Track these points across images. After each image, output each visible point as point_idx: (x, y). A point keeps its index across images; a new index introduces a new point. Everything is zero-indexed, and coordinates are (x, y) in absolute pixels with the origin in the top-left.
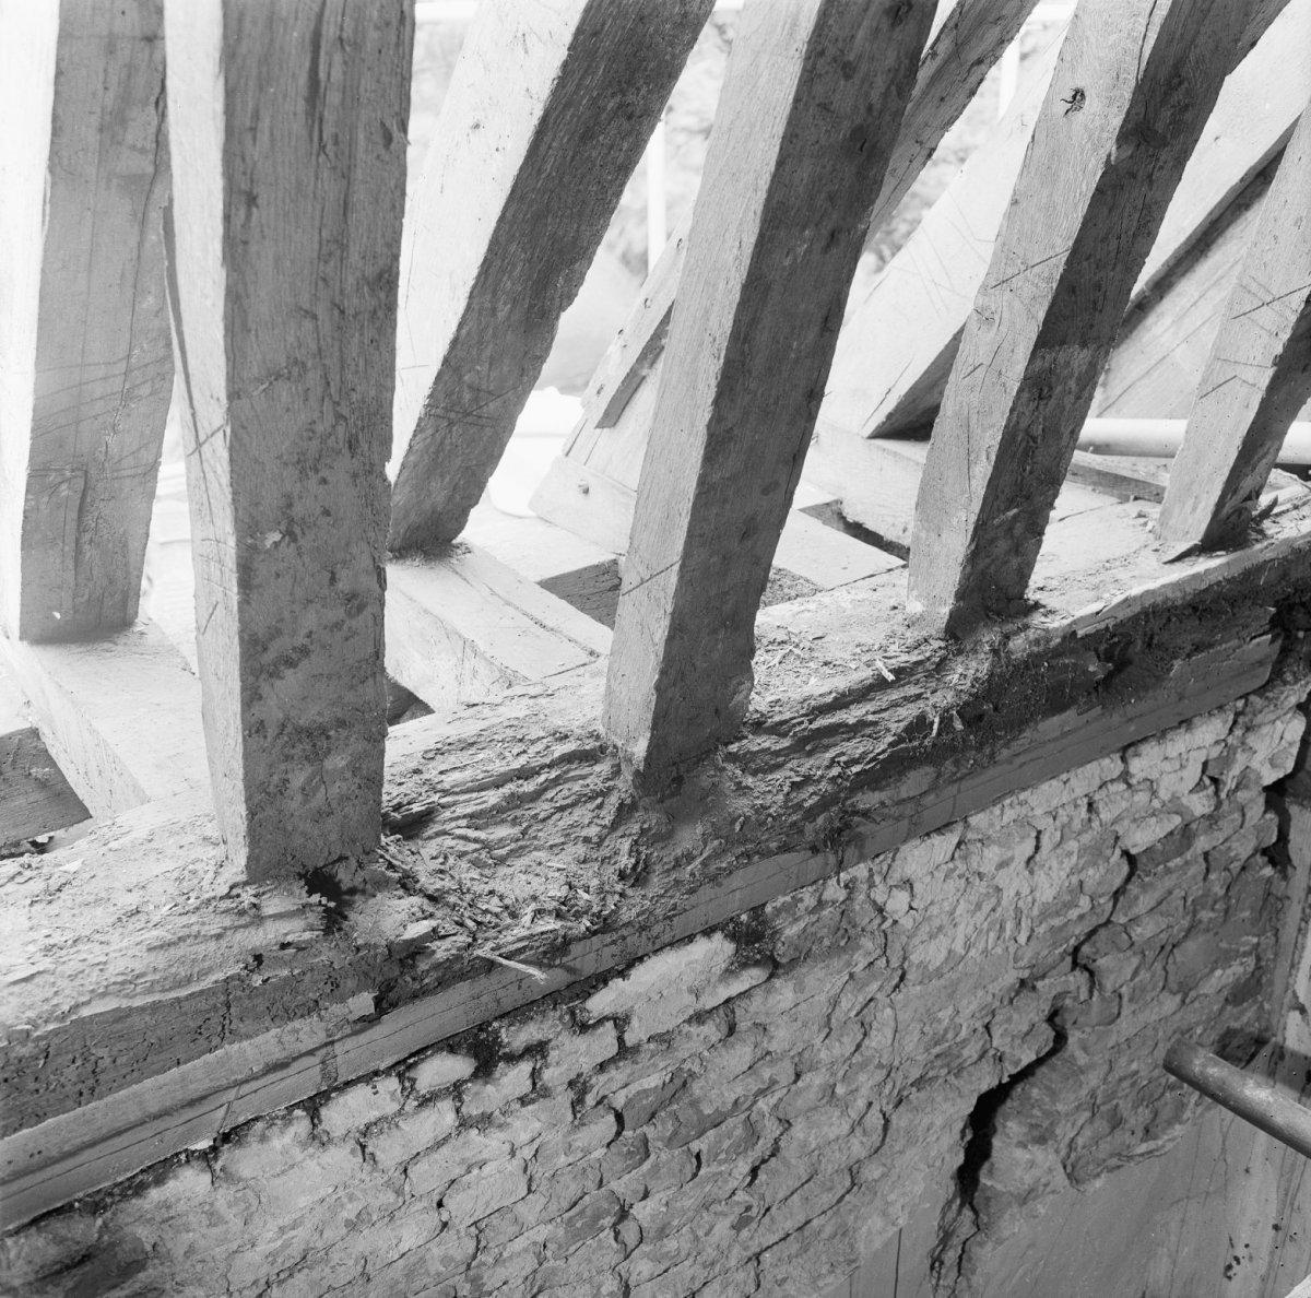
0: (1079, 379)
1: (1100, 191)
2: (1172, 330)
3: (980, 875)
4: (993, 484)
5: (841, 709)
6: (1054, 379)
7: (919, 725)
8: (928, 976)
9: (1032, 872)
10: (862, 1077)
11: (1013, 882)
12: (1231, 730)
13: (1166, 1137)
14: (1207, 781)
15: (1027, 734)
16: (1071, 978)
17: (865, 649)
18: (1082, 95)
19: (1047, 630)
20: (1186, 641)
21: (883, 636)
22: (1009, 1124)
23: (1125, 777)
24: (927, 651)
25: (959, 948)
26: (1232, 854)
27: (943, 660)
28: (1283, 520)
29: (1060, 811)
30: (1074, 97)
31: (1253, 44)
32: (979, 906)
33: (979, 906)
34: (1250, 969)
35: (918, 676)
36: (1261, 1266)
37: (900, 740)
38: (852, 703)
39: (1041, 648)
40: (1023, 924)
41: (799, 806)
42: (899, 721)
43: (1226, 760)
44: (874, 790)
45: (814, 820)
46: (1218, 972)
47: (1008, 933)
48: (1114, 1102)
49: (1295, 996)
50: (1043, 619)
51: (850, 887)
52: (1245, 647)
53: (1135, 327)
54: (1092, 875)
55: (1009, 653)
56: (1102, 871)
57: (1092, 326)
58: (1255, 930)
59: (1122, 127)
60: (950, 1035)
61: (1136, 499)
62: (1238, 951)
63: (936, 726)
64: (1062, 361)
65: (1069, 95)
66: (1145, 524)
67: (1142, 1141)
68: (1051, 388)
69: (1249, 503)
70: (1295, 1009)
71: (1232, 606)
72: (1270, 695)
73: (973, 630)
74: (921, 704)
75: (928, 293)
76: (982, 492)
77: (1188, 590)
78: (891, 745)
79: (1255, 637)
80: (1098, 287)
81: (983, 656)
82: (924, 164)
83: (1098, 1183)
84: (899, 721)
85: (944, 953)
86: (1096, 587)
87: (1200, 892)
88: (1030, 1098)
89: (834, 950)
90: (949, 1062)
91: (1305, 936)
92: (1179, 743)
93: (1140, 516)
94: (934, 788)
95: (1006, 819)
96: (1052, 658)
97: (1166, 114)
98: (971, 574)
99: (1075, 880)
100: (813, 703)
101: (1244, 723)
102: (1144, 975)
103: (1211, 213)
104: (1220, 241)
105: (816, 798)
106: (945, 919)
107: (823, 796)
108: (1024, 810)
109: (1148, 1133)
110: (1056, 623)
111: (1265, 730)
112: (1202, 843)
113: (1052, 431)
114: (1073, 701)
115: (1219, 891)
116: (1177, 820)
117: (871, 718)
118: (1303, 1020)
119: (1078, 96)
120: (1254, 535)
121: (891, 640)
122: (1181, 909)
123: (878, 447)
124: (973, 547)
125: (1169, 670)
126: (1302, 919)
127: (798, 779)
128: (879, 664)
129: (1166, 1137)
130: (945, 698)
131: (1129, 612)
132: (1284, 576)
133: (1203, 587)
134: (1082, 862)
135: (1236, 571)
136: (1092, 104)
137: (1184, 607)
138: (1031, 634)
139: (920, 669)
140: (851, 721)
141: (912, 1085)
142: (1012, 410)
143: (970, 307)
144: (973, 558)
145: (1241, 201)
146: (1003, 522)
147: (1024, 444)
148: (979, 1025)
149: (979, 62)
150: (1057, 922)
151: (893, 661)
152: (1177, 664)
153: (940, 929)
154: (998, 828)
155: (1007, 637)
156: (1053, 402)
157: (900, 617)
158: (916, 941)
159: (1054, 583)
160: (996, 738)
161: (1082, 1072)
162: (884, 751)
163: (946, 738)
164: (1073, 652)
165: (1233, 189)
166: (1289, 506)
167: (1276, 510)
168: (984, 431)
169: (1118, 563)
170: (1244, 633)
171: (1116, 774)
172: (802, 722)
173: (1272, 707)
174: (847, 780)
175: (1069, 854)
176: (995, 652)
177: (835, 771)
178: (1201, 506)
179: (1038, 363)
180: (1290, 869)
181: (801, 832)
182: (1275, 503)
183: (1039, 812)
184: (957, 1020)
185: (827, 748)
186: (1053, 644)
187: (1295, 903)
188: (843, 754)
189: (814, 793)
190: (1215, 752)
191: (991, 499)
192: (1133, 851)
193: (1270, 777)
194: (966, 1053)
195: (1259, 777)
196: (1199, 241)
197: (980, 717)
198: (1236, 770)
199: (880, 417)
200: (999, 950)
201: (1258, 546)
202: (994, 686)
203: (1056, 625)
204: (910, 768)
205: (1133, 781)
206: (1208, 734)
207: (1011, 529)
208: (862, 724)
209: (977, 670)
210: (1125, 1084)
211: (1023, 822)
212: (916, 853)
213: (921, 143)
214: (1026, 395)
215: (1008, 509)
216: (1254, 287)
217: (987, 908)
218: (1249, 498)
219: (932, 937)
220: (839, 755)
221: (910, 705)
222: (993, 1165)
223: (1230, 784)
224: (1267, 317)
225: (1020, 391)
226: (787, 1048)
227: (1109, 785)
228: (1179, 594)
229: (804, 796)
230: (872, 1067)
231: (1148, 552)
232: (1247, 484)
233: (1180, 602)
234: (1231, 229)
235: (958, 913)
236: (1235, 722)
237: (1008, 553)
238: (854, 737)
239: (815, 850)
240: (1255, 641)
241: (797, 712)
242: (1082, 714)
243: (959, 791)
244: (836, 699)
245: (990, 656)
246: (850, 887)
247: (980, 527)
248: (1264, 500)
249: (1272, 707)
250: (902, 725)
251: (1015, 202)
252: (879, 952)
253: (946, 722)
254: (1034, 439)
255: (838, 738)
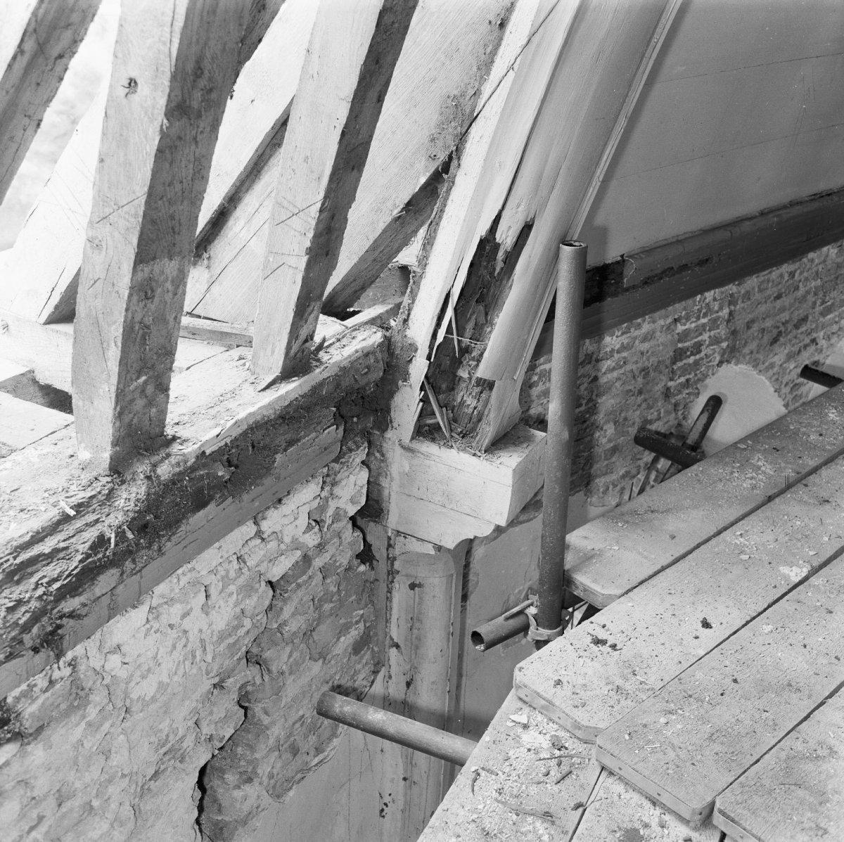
0: (173, 281)
1: (160, 151)
2: (246, 228)
3: (171, 626)
4: (123, 362)
5: (37, 543)
6: (154, 284)
7: (101, 541)
8: (145, 704)
9: (207, 614)
10: (111, 789)
11: (197, 623)
12: (322, 488)
13: (329, 749)
14: (314, 524)
15: (183, 528)
16: (248, 672)
17: (51, 492)
18: (135, 82)
19: (184, 455)
20: (281, 440)
21: (64, 480)
22: (226, 776)
23: (259, 534)
24: (98, 486)
25: (166, 680)
26: (338, 564)
27: (111, 491)
28: (332, 350)
29: (219, 568)
30: (130, 84)
31: (260, 41)
32: (174, 647)
33: (174, 647)
34: (362, 631)
35: (94, 507)
36: (401, 803)
37: (88, 556)
38: (46, 537)
39: (182, 468)
40: (207, 648)
41: (16, 624)
42: (84, 543)
43: (322, 508)
44: (73, 597)
45: (30, 631)
46: (342, 639)
47: (198, 658)
48: (292, 739)
49: (392, 639)
50: (181, 447)
51: (73, 664)
52: (321, 437)
53: (221, 228)
54: (250, 603)
55: (158, 477)
56: (255, 599)
57: (174, 244)
58: (361, 606)
59: (167, 106)
60: (171, 738)
61: (238, 346)
62: (351, 622)
63: (113, 541)
64: (158, 272)
65: (126, 83)
66: (244, 365)
67: (315, 756)
68: (153, 291)
69: (307, 344)
70: (392, 646)
71: (308, 412)
72: (343, 460)
73: (131, 465)
74: (99, 526)
75: (69, 218)
76: (116, 369)
77: (277, 408)
78: (81, 561)
79: (326, 429)
80: (172, 217)
81: (140, 482)
82: (36, 131)
83: (291, 793)
84: (84, 543)
85: (155, 686)
86: (214, 417)
87: (322, 593)
88: (237, 754)
89: (71, 709)
90: (175, 754)
91: (391, 601)
92: (290, 505)
93: (241, 358)
94: (121, 581)
95: (182, 583)
96: (190, 473)
97: (198, 95)
98: (120, 428)
99: (238, 610)
100: (15, 544)
101: (330, 481)
102: (295, 655)
103: (257, 151)
104: (266, 168)
105: (28, 615)
106: (152, 664)
107: (34, 612)
108: (194, 574)
109: (319, 750)
110: (190, 449)
111: (344, 483)
112: (318, 562)
113: (161, 319)
114: (211, 498)
115: (333, 589)
116: (298, 553)
117: (62, 545)
118: (398, 651)
119: (132, 83)
120: (314, 363)
121: (71, 482)
122: (312, 607)
123: (52, 330)
124: (118, 409)
125: (274, 462)
126: (388, 592)
127: (11, 604)
128: (62, 504)
129: (329, 749)
130: (116, 518)
131: (239, 431)
132: (338, 386)
133: (287, 403)
134: (240, 597)
135: (306, 389)
136: (143, 89)
137: (276, 419)
138: (173, 460)
139: (94, 501)
140: (47, 551)
141: (150, 780)
142: (127, 310)
143: (84, 238)
144: (119, 416)
145: (275, 141)
146: (136, 388)
147: (141, 332)
148: (191, 723)
149: (61, 56)
150: (231, 640)
151: (73, 499)
152: (279, 457)
153: (149, 670)
154: (177, 591)
155: (155, 466)
156: (156, 300)
157: (76, 463)
158: (132, 684)
159: (186, 418)
160: (159, 537)
161: (268, 729)
162: (76, 567)
163: (123, 547)
164: (205, 466)
165: (267, 135)
166: (334, 340)
167: (326, 344)
168: (109, 325)
169: (229, 396)
170: (319, 428)
171: (252, 534)
172: (8, 560)
173: (345, 468)
174: (51, 595)
175: (231, 595)
176: (148, 478)
177: (40, 591)
178: (277, 351)
179: (140, 276)
180: (375, 562)
181: (21, 642)
182: (324, 340)
183: (204, 573)
184: (174, 726)
185: (32, 574)
186: (189, 464)
187: (382, 581)
188: (45, 577)
189: (26, 612)
190: (315, 504)
191: (124, 373)
192: (274, 580)
193: (352, 510)
194: (185, 745)
195: (346, 512)
196: (253, 169)
197: (145, 526)
198: (330, 512)
199: (50, 309)
200: (194, 671)
201: (318, 370)
202: (152, 504)
203: (189, 450)
204: (98, 574)
205: (265, 536)
206: (306, 496)
207: (143, 391)
208: (56, 551)
209: (138, 493)
210: (298, 725)
211: (194, 583)
212: (119, 625)
213: (29, 117)
214: (135, 298)
215: (138, 378)
216: (285, 204)
217: (179, 646)
218: (306, 341)
219: (143, 677)
220: (41, 579)
221: (93, 529)
222: (220, 805)
223: (329, 521)
224: (296, 223)
225: (130, 295)
226: (46, 790)
227: (249, 542)
228: (271, 411)
229: (19, 616)
230: (117, 779)
231: (247, 385)
232: (303, 333)
233: (273, 416)
234: (271, 160)
235: (159, 656)
236: (324, 482)
237: (145, 407)
238: (51, 562)
239: (36, 650)
240: (326, 432)
241: (3, 552)
242: (218, 505)
243: (141, 577)
244: (32, 536)
245: (146, 481)
246: (73, 664)
247: (120, 395)
248: (317, 339)
249: (345, 468)
250: (87, 545)
251: (102, 161)
252: (106, 701)
253: (120, 535)
254: (148, 327)
255: (39, 565)
